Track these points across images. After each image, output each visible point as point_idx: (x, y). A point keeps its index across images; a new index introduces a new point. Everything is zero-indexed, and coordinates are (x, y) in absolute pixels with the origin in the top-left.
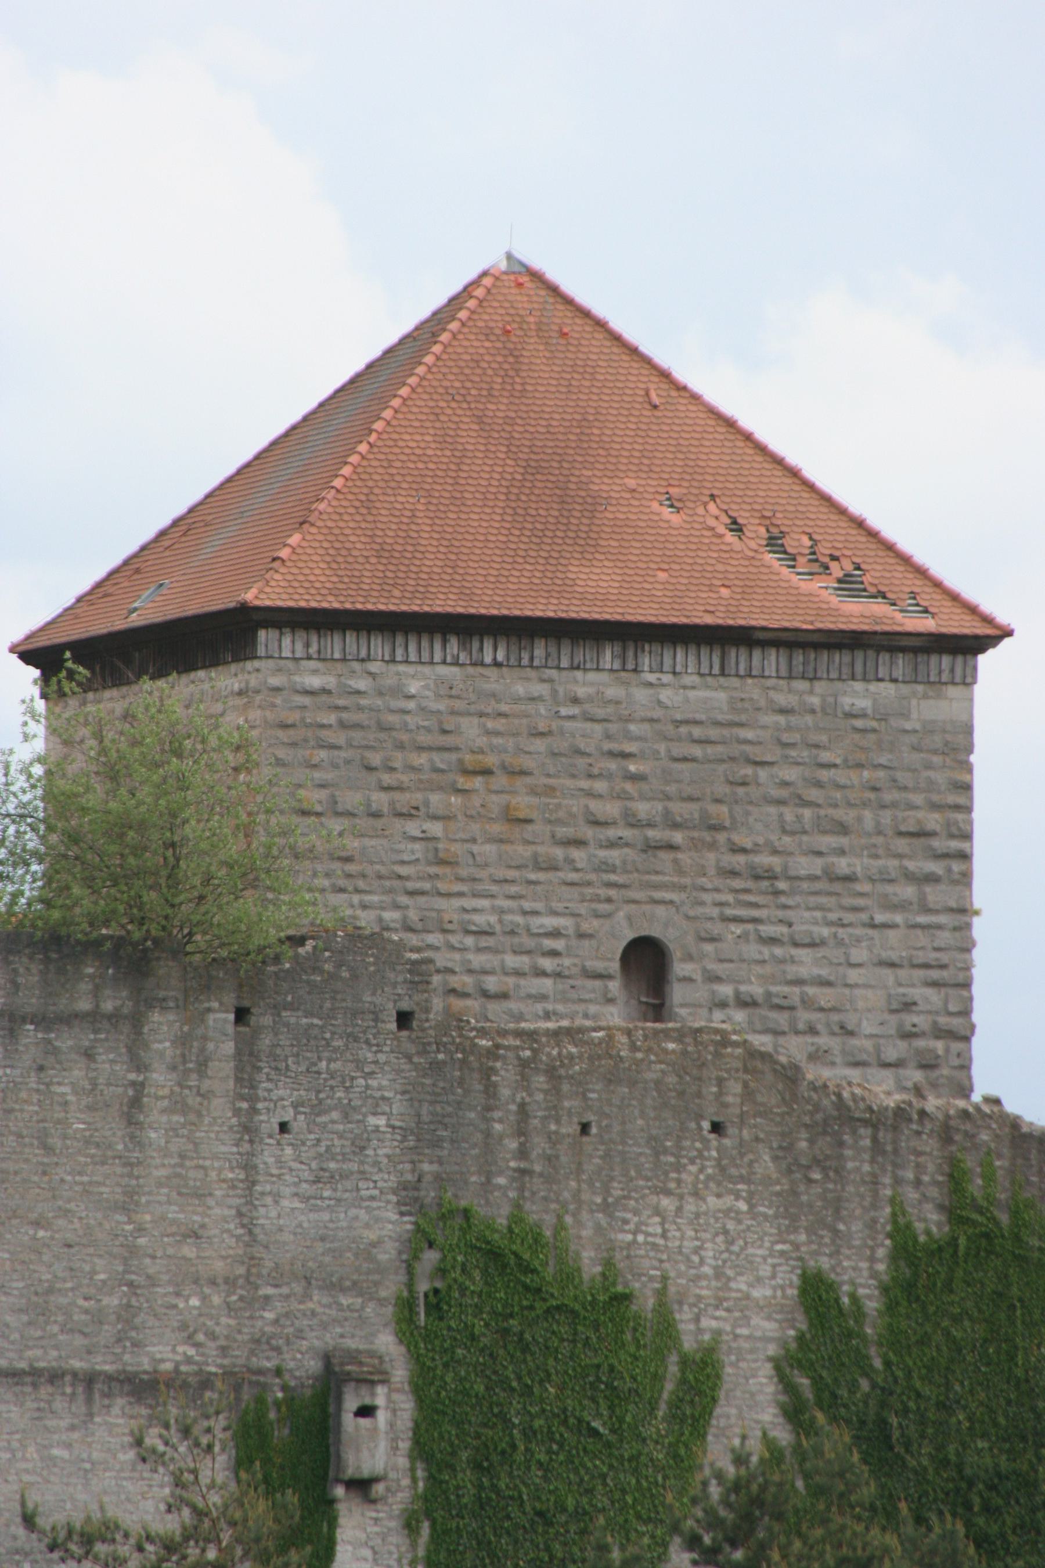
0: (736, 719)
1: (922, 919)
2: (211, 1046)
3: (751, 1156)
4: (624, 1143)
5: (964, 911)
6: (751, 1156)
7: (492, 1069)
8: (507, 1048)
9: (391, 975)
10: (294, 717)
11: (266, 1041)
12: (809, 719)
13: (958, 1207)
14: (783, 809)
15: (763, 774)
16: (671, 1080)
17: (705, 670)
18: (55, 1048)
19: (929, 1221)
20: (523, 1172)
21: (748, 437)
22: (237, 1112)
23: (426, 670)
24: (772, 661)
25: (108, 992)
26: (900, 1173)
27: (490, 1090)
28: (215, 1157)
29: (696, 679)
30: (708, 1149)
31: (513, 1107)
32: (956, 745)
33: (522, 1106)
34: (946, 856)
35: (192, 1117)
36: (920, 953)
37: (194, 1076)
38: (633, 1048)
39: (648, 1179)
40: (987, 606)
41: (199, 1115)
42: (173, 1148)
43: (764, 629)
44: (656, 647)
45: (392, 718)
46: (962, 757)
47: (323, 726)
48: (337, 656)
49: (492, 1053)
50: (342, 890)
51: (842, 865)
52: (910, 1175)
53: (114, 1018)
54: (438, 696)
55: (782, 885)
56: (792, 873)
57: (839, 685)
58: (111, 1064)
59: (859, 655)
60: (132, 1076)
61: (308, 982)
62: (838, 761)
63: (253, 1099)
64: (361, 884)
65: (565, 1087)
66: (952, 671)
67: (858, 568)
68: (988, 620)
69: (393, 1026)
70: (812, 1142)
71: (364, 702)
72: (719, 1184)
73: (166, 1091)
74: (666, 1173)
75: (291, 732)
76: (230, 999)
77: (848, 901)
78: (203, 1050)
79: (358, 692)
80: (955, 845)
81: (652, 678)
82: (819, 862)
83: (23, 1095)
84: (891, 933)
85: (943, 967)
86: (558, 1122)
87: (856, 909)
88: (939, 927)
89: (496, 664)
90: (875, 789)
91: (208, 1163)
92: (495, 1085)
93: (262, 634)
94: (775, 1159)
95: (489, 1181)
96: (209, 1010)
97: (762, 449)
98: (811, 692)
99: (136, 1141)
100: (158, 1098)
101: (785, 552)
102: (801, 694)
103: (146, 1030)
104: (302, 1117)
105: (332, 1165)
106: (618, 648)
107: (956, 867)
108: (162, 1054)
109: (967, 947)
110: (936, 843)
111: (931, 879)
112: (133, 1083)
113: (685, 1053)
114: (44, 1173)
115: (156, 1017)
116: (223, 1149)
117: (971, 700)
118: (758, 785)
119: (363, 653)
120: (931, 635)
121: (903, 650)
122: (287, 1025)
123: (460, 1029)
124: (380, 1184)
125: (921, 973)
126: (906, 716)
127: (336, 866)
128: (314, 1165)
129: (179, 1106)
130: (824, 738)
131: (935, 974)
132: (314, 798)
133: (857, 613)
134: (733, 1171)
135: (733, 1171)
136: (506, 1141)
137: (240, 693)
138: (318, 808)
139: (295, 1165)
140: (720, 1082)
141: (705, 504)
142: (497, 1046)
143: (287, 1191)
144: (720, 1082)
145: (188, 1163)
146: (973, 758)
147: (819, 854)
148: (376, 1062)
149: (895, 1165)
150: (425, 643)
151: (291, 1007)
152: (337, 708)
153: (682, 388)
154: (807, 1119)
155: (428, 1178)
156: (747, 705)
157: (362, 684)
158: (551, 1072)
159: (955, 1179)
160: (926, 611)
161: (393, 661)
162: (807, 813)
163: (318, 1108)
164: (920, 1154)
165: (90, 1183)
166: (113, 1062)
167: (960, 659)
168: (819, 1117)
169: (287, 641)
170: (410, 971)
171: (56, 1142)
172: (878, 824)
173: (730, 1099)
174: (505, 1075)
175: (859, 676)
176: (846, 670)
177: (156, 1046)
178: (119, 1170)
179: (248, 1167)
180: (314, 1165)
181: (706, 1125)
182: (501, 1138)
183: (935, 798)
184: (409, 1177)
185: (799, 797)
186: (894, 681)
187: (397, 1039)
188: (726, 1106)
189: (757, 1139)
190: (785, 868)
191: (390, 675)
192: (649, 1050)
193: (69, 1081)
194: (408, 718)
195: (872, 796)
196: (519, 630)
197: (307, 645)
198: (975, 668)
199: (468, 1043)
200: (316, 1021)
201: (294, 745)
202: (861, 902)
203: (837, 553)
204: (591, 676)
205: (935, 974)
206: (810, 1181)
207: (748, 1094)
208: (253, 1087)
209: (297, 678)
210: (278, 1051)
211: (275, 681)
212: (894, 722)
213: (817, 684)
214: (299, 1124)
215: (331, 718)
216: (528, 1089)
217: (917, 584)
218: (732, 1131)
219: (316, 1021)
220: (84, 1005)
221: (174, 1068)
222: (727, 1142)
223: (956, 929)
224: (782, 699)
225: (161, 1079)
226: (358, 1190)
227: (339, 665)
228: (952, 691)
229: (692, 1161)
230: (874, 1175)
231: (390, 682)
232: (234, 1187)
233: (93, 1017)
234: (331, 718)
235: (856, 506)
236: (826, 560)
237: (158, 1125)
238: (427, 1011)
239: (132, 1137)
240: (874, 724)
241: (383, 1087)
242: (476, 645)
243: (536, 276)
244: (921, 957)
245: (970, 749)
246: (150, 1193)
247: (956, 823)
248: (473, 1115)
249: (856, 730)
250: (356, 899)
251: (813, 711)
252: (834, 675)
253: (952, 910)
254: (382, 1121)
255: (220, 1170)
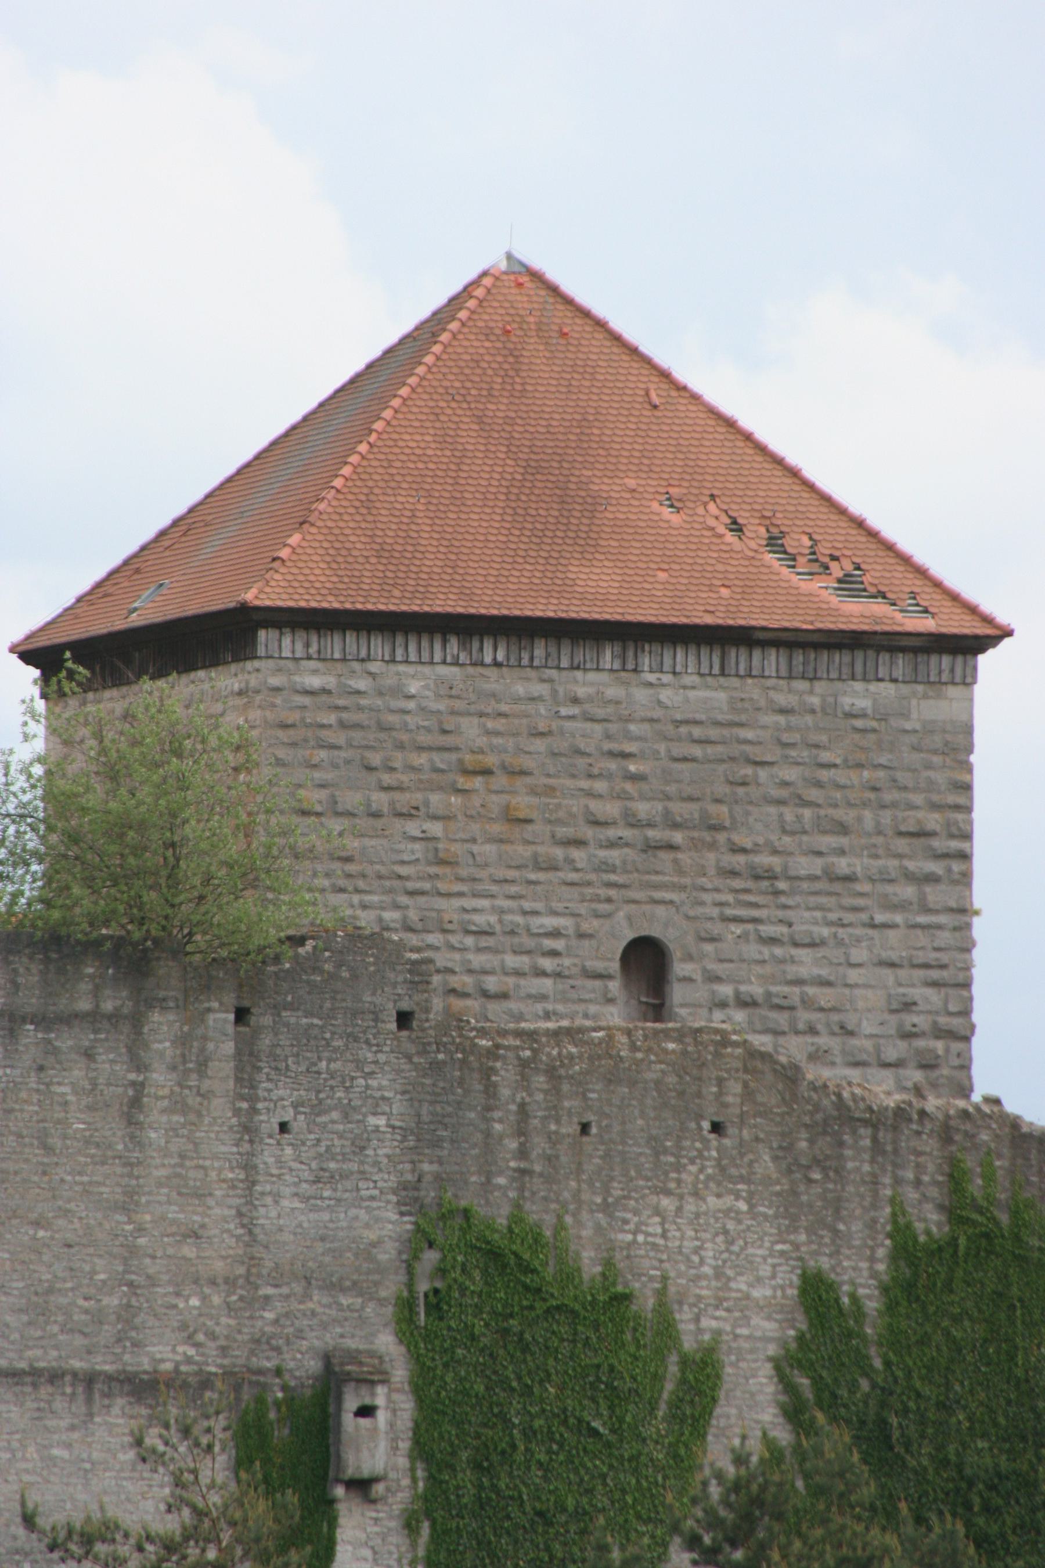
0: (736, 719)
1: (922, 919)
2: (211, 1046)
3: (751, 1156)
4: (624, 1143)
5: (964, 911)
6: (751, 1156)
7: (492, 1069)
8: (507, 1048)
9: (391, 975)
10: (294, 717)
11: (266, 1041)
12: (809, 719)
13: (958, 1207)
14: (783, 809)
15: (763, 774)
16: (671, 1080)
17: (705, 670)
18: (55, 1048)
19: (929, 1221)
20: (523, 1172)
21: (748, 437)
22: (237, 1112)
23: (426, 670)
24: (772, 661)
25: (108, 992)
26: (900, 1173)
27: (490, 1090)
28: (215, 1157)
29: (696, 679)
30: (708, 1149)
31: (513, 1107)
32: (956, 745)
33: (522, 1106)
34: (946, 856)
35: (192, 1117)
36: (920, 953)
37: (194, 1076)
38: (633, 1048)
39: (648, 1179)
40: (987, 606)
41: (199, 1115)
42: (173, 1148)
43: (764, 629)
44: (656, 647)
45: (392, 718)
46: (962, 757)
47: (323, 726)
48: (337, 656)
49: (492, 1053)
50: (342, 890)
51: (842, 865)
52: (910, 1175)
53: (114, 1018)
54: (438, 696)
55: (782, 885)
56: (792, 873)
57: (839, 685)
58: (111, 1064)
59: (859, 655)
60: (132, 1076)
61: (308, 982)
62: (838, 761)
63: (253, 1099)
64: (361, 884)
65: (565, 1087)
66: (952, 671)
67: (858, 568)
68: (988, 620)
69: (393, 1026)
70: (812, 1142)
71: (364, 702)
72: (719, 1184)
73: (166, 1091)
74: (666, 1173)
75: (291, 732)
76: (230, 999)
77: (848, 901)
78: (203, 1050)
79: (358, 692)
80: (955, 845)
81: (652, 678)
82: (819, 862)
83: (23, 1095)
84: (891, 933)
85: (943, 967)
86: (558, 1122)
87: (856, 909)
88: (939, 927)
89: (496, 664)
90: (875, 789)
91: (208, 1163)
92: (495, 1085)
93: (262, 634)
94: (775, 1159)
95: (489, 1181)
96: (209, 1010)
97: (762, 449)
98: (811, 692)
99: (136, 1141)
100: (158, 1098)
101: (785, 552)
102: (801, 694)
103: (146, 1030)
104: (302, 1117)
105: (332, 1165)
106: (618, 648)
107: (956, 867)
108: (162, 1054)
109: (967, 947)
110: (936, 843)
111: (931, 879)
112: (133, 1083)
113: (685, 1053)
114: (44, 1173)
115: (156, 1017)
116: (223, 1149)
117: (971, 700)
118: (758, 785)
119: (363, 653)
120: (931, 635)
121: (903, 650)
122: (287, 1025)
123: (460, 1029)
124: (380, 1184)
125: (921, 973)
126: (906, 716)
127: (336, 866)
128: (314, 1165)
129: (179, 1106)
130: (824, 738)
131: (935, 974)
132: (314, 798)
133: (857, 613)
134: (733, 1171)
135: (733, 1171)
136: (506, 1141)
137: (240, 693)
138: (318, 808)
139: (295, 1165)
140: (720, 1082)
141: (705, 504)
142: (497, 1046)
143: (287, 1191)
144: (720, 1082)
145: (188, 1163)
146: (973, 758)
147: (819, 854)
148: (376, 1062)
149: (895, 1165)
150: (425, 643)
151: (291, 1007)
152: (337, 708)
153: (682, 388)
154: (807, 1119)
155: (428, 1178)
156: (747, 705)
157: (362, 684)
158: (551, 1072)
159: (955, 1179)
160: (926, 611)
161: (393, 661)
162: (807, 813)
163: (318, 1108)
164: (920, 1154)
165: (90, 1183)
166: (113, 1062)
167: (960, 659)
168: (819, 1117)
169: (287, 641)
170: (410, 971)
171: (56, 1142)
172: (878, 824)
173: (730, 1099)
174: (505, 1075)
175: (859, 676)
176: (846, 670)
177: (156, 1046)
178: (119, 1170)
179: (248, 1167)
180: (314, 1165)
181: (706, 1125)
182: (501, 1138)
183: (935, 798)
184: (409, 1177)
185: (799, 797)
186: (894, 681)
187: (397, 1039)
188: (726, 1106)
189: (757, 1139)
190: (785, 868)
191: (390, 675)
192: (649, 1050)
193: (69, 1081)
194: (408, 718)
195: (872, 796)
196: (519, 630)
197: (307, 645)
198: (975, 668)
199: (468, 1043)
200: (316, 1021)
201: (294, 745)
202: (861, 902)
203: (837, 553)
204: (591, 676)
205: (935, 974)
206: (810, 1181)
207: (748, 1094)
208: (253, 1087)
209: (297, 678)
210: (278, 1051)
211: (275, 681)
212: (894, 722)
213: (817, 684)
214: (299, 1124)
215: (331, 718)
216: (528, 1089)
217: (917, 584)
218: (732, 1131)
219: (316, 1021)
220: (84, 1005)
221: (174, 1068)
222: (727, 1142)
223: (956, 929)
224: (782, 699)
225: (161, 1079)
226: (358, 1190)
227: (339, 665)
228: (952, 691)
229: (692, 1161)
230: (874, 1175)
231: (390, 682)
232: (234, 1187)
233: (93, 1017)
234: (331, 718)
235: (856, 506)
236: (826, 560)
237: (158, 1125)
238: (427, 1011)
239: (132, 1137)
240: (874, 724)
241: (383, 1087)
242: (476, 645)
243: (536, 276)
244: (921, 957)
245: (970, 749)
246: (150, 1193)
247: (956, 823)
248: (473, 1115)
249: (856, 730)
250: (356, 899)
251: (813, 711)
252: (834, 675)
253: (952, 910)
254: (382, 1121)
255: (220, 1170)
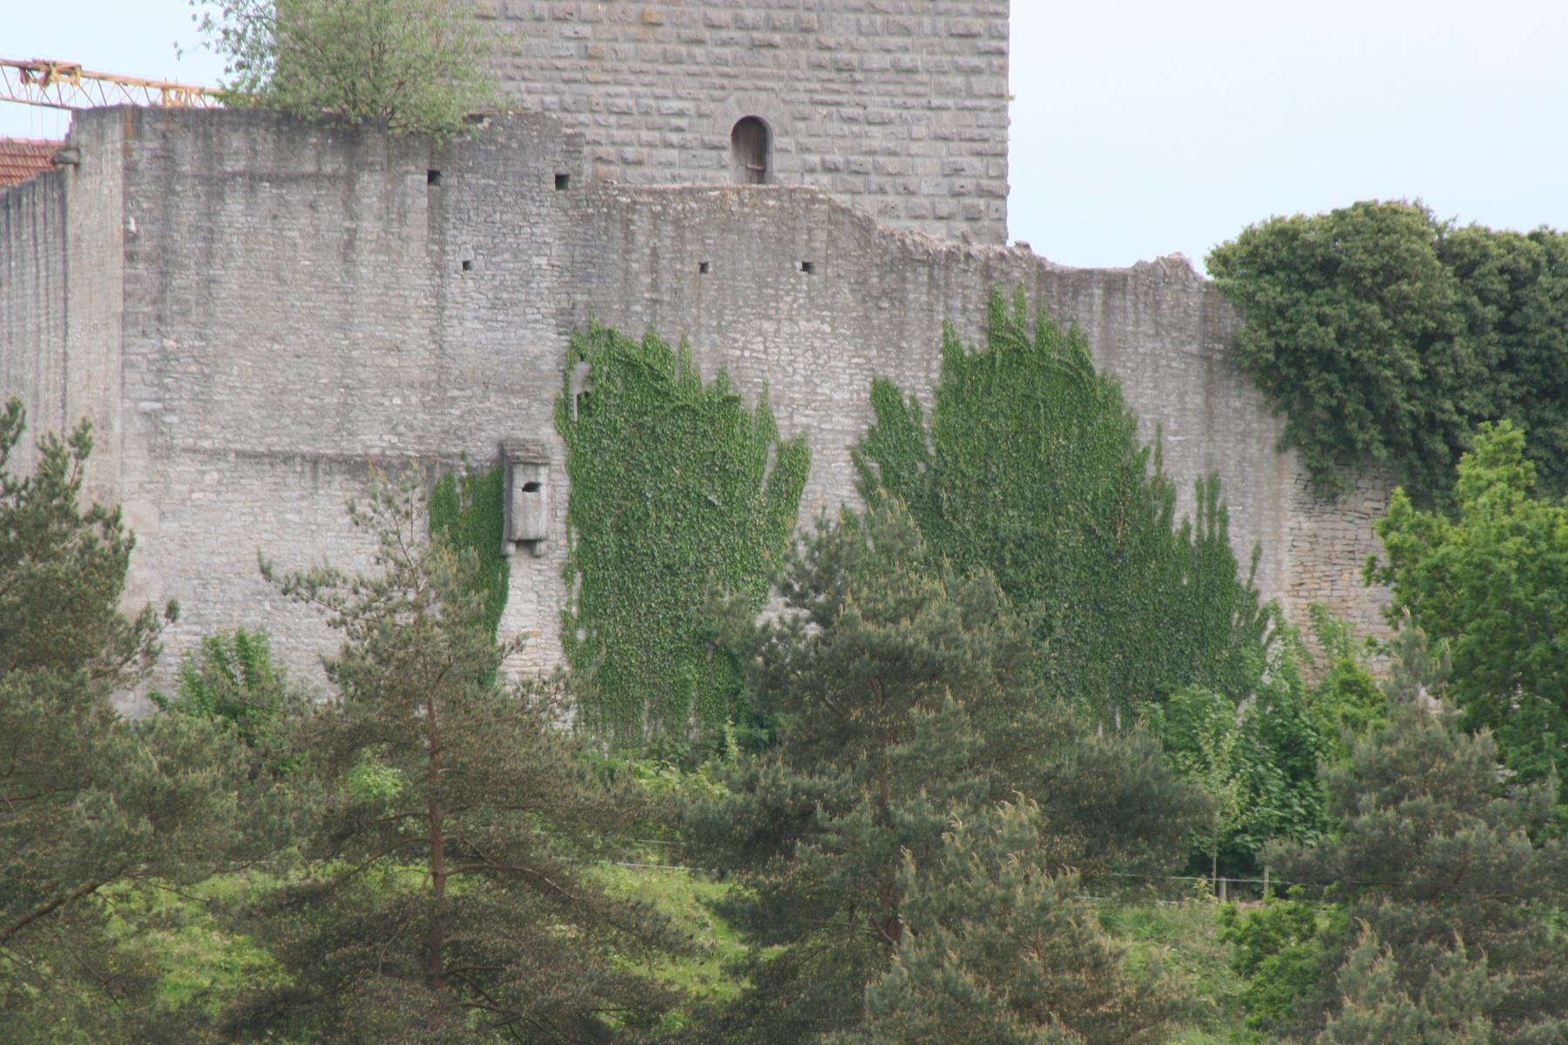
1: (968, 103)
2: (409, 201)
4: (734, 279)
8: (643, 204)
11: (452, 197)
16: (772, 229)
19: (973, 340)
22: (430, 253)
25: (328, 158)
27: (629, 236)
28: (413, 288)
31: (647, 251)
35: (394, 257)
36: (967, 130)
37: (396, 224)
38: (742, 204)
39: (753, 307)
41: (400, 254)
49: (631, 208)
50: (512, 79)
51: (906, 60)
52: (958, 304)
53: (333, 178)
55: (858, 76)
56: (866, 66)
58: (330, 214)
60: (347, 224)
63: (442, 243)
64: (527, 74)
65: (688, 235)
69: (553, 186)
70: (881, 278)
72: (808, 311)
74: (767, 303)
77: (911, 89)
78: (403, 203)
80: (994, 44)
83: (261, 238)
84: (945, 114)
85: (985, 140)
86: (682, 262)
87: (917, 95)
88: (982, 109)
94: (853, 291)
95: (628, 308)
96: (407, 172)
100: (367, 242)
105: (505, 295)
107: (996, 61)
108: (370, 207)
110: (980, 43)
111: (976, 71)
112: (348, 230)
113: (782, 208)
115: (365, 177)
116: (420, 282)
122: (469, 185)
123: (605, 188)
125: (967, 145)
127: (508, 59)
131: (979, 146)
135: (820, 301)
136: (642, 277)
139: (476, 295)
140: (810, 231)
142: (635, 203)
143: (469, 315)
144: (810, 231)
147: (888, 51)
148: (539, 215)
149: (947, 296)
154: (877, 260)
155: (580, 306)
158: (677, 222)
159: (993, 307)
162: (879, 19)
163: (494, 251)
164: (967, 287)
168: (887, 258)
171: (287, 275)
172: (934, 27)
173: (818, 245)
174: (641, 224)
178: (337, 298)
179: (439, 296)
181: (799, 265)
184: (565, 305)
188: (814, 250)
190: (861, 62)
193: (297, 228)
202: (921, 89)
205: (979, 146)
206: (880, 309)
207: (832, 240)
214: (479, 262)
216: (658, 236)
218: (818, 269)
220: (309, 168)
222: (815, 278)
225: (369, 227)
229: (788, 293)
233: (316, 177)
238: (579, 174)
239: (347, 272)
241: (545, 230)
244: (967, 133)
247: (996, 27)
250: (523, 85)
253: (992, 96)
254: (543, 261)
255: (417, 299)
